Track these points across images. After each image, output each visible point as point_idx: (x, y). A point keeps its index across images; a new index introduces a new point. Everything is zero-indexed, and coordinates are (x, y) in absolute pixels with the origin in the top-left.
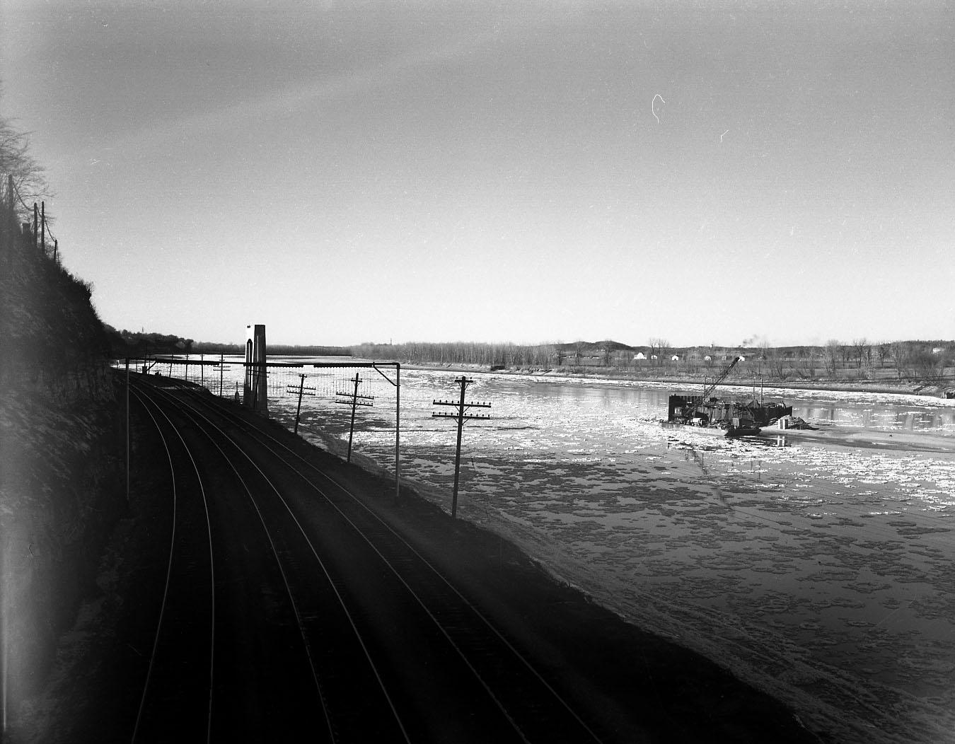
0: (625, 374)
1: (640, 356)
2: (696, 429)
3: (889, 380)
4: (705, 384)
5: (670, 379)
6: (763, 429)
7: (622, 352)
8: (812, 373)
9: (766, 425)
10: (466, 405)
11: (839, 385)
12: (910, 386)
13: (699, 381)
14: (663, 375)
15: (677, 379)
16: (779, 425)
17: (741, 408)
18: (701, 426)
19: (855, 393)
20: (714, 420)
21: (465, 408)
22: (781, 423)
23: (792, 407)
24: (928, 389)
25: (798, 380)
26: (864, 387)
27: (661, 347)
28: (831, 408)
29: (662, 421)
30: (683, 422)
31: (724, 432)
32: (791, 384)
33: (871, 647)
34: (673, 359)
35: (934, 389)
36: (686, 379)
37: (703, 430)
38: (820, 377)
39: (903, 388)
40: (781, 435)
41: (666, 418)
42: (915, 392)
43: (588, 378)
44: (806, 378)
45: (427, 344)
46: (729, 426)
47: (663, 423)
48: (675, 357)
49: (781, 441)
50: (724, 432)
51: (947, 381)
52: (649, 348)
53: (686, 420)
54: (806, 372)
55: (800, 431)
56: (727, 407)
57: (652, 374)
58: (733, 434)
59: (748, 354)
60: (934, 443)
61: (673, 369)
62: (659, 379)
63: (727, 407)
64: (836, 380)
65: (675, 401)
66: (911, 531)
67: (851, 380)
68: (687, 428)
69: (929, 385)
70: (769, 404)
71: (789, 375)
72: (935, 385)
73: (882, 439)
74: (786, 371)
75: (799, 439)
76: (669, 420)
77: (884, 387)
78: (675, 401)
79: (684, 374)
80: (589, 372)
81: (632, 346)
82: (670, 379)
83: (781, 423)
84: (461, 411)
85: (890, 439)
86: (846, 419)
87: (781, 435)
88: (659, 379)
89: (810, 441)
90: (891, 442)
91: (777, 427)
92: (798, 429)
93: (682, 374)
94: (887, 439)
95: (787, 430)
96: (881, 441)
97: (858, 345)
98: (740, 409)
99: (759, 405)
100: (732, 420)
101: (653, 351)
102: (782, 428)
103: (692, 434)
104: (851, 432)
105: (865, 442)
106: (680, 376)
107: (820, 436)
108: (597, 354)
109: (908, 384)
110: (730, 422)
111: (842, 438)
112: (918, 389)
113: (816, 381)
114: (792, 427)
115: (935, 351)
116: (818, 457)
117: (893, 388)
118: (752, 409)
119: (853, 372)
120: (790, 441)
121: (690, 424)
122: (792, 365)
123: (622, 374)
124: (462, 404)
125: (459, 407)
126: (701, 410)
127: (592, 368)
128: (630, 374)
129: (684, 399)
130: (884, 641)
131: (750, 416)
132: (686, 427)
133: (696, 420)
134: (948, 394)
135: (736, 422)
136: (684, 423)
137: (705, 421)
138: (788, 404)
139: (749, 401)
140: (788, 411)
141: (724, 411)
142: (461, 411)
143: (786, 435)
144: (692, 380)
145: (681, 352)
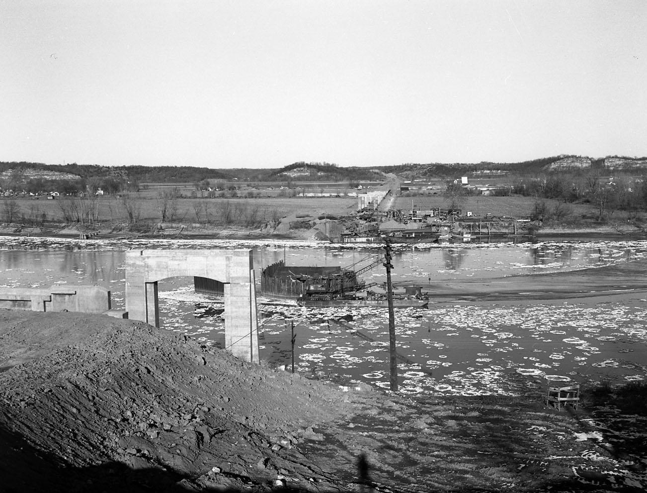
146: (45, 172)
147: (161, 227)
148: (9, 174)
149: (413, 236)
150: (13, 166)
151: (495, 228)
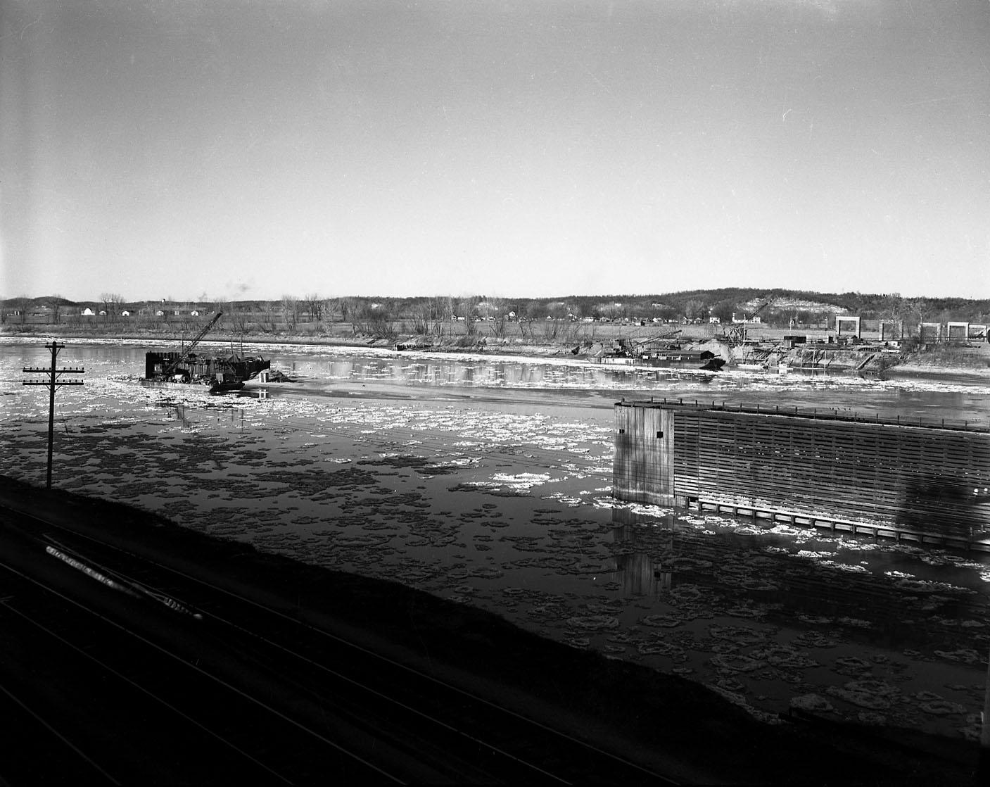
0: (80, 331)
1: (88, 312)
2: (179, 385)
3: (345, 334)
4: (183, 340)
5: (130, 335)
6: (245, 382)
7: (68, 309)
8: (274, 327)
9: (247, 379)
10: (58, 372)
11: (300, 339)
12: (364, 339)
13: (160, 337)
14: (121, 331)
15: (137, 336)
16: (260, 379)
17: (222, 364)
18: (184, 382)
19: (262, 344)
20: (196, 375)
21: (57, 374)
22: (262, 376)
23: (269, 361)
24: (379, 342)
25: (260, 334)
26: (322, 340)
27: (115, 302)
28: (291, 360)
29: (142, 380)
30: (164, 379)
31: (209, 387)
32: (254, 338)
33: (541, 611)
34: (124, 314)
35: (385, 342)
36: (147, 335)
37: (186, 386)
38: (281, 331)
39: (359, 341)
40: (263, 388)
41: (144, 376)
42: (369, 345)
43: (38, 337)
44: (268, 332)
45: (292, 299)
46: (213, 381)
47: (142, 381)
48: (88, 312)
49: (262, 395)
50: (209, 387)
51: (396, 335)
52: (102, 303)
53: (168, 376)
54: (268, 326)
55: (281, 384)
56: (208, 362)
57: (110, 331)
58: (218, 389)
59: (200, 309)
60: (402, 391)
61: (132, 325)
62: (118, 335)
63: (208, 362)
64: (296, 333)
65: (153, 359)
66: (763, 487)
67: (311, 333)
68: (170, 385)
69: (381, 338)
70: (248, 358)
71: (252, 329)
72: (386, 338)
73: (356, 389)
74: (247, 325)
75: (278, 392)
76: (147, 377)
77: (341, 340)
78: (153, 359)
79: (144, 330)
80: (39, 331)
81: (76, 301)
82: (130, 335)
83: (262, 376)
84: (53, 377)
85: (363, 389)
86: (305, 370)
87: (263, 388)
88: (118, 335)
89: (293, 393)
90: (365, 392)
91: (258, 380)
92: (279, 382)
93: (142, 330)
94: (359, 389)
95: (268, 383)
96: (357, 391)
97: (310, 300)
98: (221, 364)
99: (239, 359)
100: (215, 375)
101: (106, 306)
102: (263, 381)
103: (176, 390)
104: (327, 383)
105: (342, 392)
106: (140, 332)
107: (300, 388)
108: (37, 311)
109: (362, 337)
110: (214, 378)
111: (321, 389)
112: (371, 342)
113: (278, 335)
114: (273, 380)
115: (374, 306)
116: (304, 407)
117: (349, 341)
118: (233, 363)
119: (312, 326)
120: (271, 393)
121: (173, 381)
122: (250, 320)
123: (77, 332)
124: (53, 370)
125: (50, 374)
126: (181, 366)
127: (42, 326)
128: (85, 331)
129: (160, 356)
130: (552, 604)
131: (231, 371)
132: (168, 384)
133: (178, 377)
134: (398, 346)
135: (220, 377)
136: (166, 380)
137: (188, 379)
138: (266, 359)
139: (229, 356)
140: (266, 365)
141: (205, 367)
142: (53, 377)
143: (267, 388)
144: (153, 336)
145: (134, 308)
146: (801, 303)
147: (485, 342)
148: (755, 305)
149: (679, 359)
150: (761, 294)
151: (841, 360)
